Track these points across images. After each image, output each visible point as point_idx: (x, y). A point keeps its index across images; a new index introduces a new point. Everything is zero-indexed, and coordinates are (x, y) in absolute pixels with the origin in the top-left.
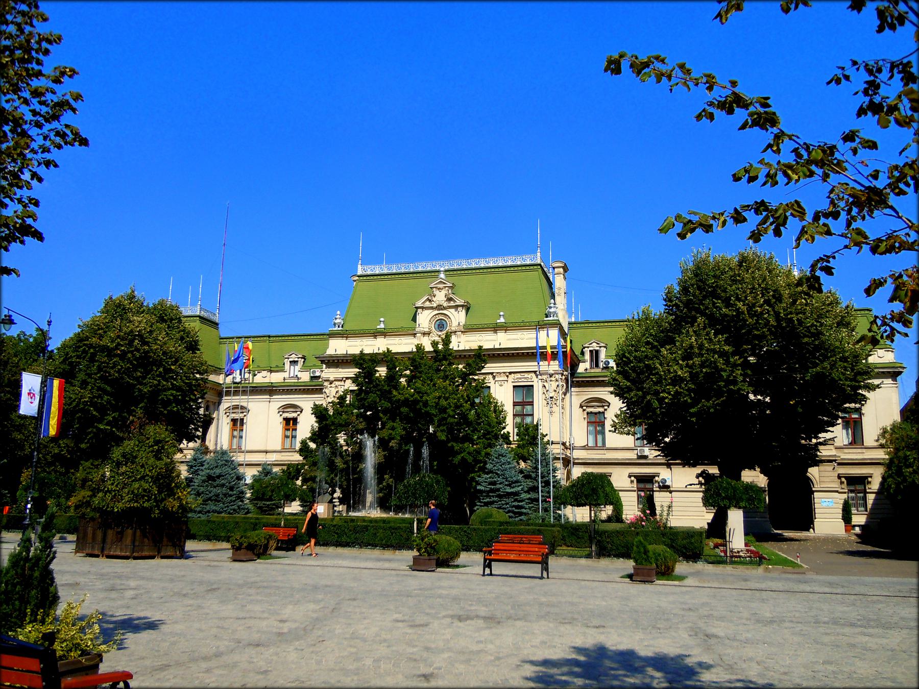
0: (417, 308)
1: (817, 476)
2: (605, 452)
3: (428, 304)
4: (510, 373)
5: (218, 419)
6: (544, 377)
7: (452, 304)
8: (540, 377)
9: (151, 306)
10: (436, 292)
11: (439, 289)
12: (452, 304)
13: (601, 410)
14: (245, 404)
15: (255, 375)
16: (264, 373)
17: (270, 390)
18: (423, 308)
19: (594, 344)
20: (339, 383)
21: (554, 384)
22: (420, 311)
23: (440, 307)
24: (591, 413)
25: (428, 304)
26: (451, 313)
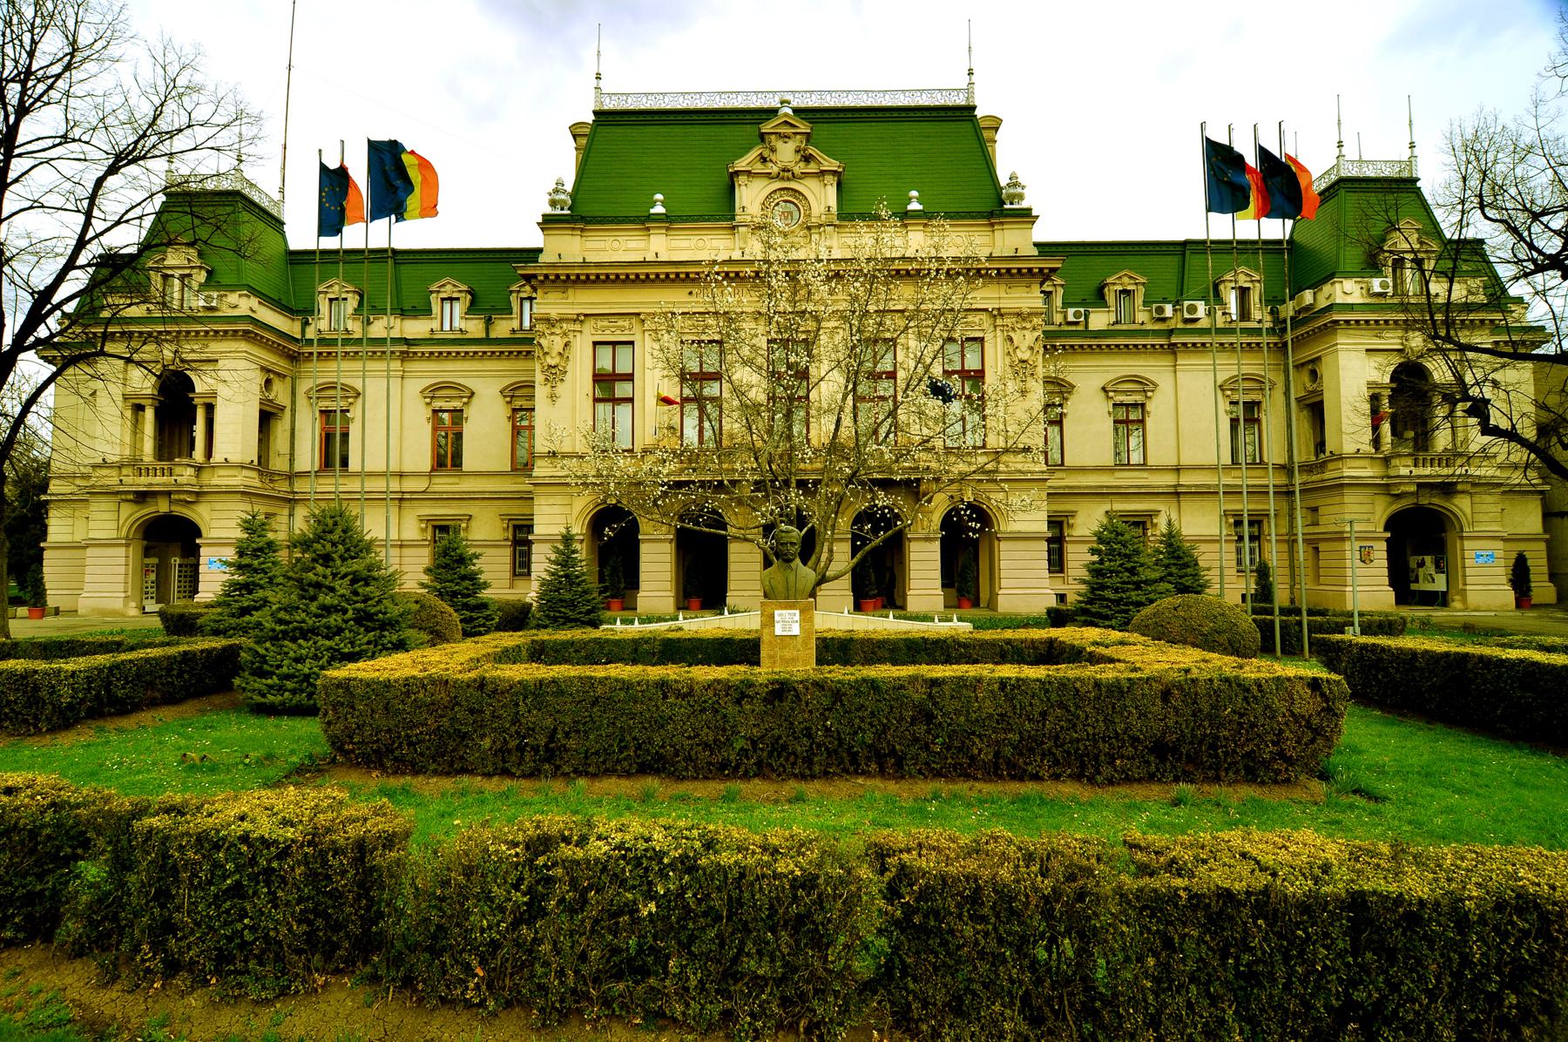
0: (737, 173)
1: (1468, 511)
2: (1145, 474)
3: (759, 168)
4: (580, 319)
5: (293, 411)
6: (1008, 321)
7: (812, 168)
8: (999, 321)
9: (426, 579)
10: (779, 145)
11: (787, 136)
12: (812, 168)
13: (1139, 398)
14: (357, 384)
15: (369, 323)
17: (407, 349)
18: (749, 173)
19: (1126, 280)
20: (572, 327)
21: (1030, 337)
22: (742, 179)
23: (786, 173)
24: (1121, 405)
25: (759, 168)
26: (809, 188)
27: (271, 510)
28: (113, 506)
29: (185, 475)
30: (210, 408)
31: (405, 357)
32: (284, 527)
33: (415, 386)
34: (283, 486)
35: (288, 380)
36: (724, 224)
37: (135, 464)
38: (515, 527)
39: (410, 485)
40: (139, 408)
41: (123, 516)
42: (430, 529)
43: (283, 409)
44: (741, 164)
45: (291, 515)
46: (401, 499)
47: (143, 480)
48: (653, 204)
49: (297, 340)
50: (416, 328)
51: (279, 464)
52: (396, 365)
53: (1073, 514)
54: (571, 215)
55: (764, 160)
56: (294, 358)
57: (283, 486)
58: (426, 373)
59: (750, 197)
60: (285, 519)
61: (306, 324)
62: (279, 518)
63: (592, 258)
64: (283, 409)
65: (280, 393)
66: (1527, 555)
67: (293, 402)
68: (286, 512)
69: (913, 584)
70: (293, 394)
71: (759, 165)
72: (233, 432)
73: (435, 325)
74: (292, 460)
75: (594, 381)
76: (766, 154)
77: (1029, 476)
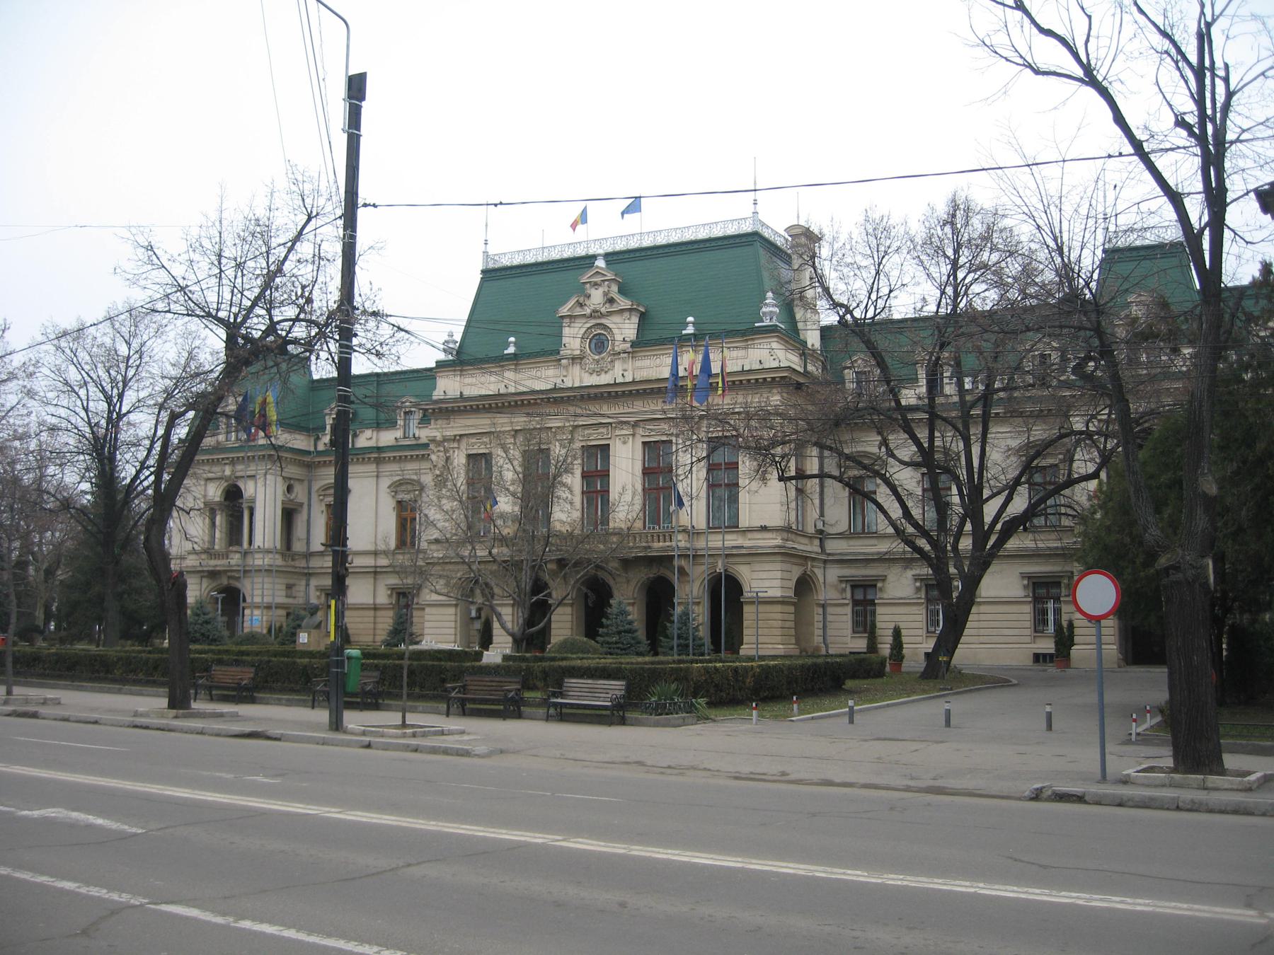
3: (578, 311)
4: (458, 438)
5: (309, 505)
11: (596, 284)
16: (368, 433)
18: (570, 317)
23: (596, 314)
25: (578, 311)
27: (291, 582)
28: (198, 580)
29: (235, 559)
30: (252, 512)
31: (378, 461)
32: (302, 594)
33: (385, 483)
34: (303, 563)
35: (306, 483)
36: (553, 358)
37: (209, 552)
38: (399, 594)
39: (383, 561)
40: (213, 513)
41: (204, 586)
42: (849, 589)
43: (301, 505)
44: (564, 311)
45: (308, 585)
46: (375, 573)
47: (213, 562)
48: (507, 345)
49: (309, 453)
50: (387, 438)
51: (298, 546)
52: (373, 467)
53: (884, 579)
54: (461, 359)
55: (581, 305)
56: (309, 466)
57: (303, 563)
58: (392, 472)
59: (573, 338)
60: (303, 588)
61: (318, 439)
62: (297, 588)
63: (467, 393)
64: (301, 505)
65: (300, 493)
66: (902, 625)
67: (310, 500)
68: (303, 583)
69: (569, 625)
70: (310, 493)
71: (578, 309)
72: (265, 527)
73: (399, 434)
74: (308, 543)
75: (644, 474)
76: (581, 300)
77: (744, 551)
